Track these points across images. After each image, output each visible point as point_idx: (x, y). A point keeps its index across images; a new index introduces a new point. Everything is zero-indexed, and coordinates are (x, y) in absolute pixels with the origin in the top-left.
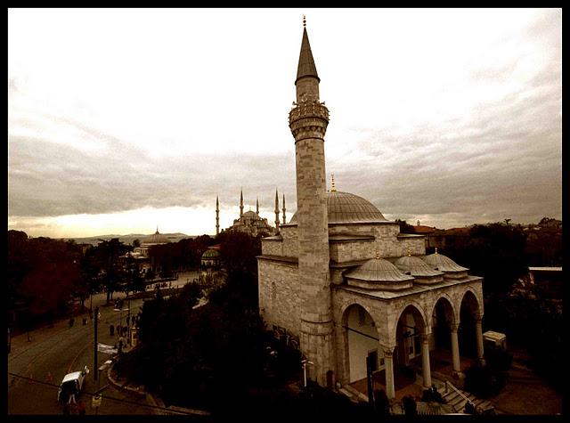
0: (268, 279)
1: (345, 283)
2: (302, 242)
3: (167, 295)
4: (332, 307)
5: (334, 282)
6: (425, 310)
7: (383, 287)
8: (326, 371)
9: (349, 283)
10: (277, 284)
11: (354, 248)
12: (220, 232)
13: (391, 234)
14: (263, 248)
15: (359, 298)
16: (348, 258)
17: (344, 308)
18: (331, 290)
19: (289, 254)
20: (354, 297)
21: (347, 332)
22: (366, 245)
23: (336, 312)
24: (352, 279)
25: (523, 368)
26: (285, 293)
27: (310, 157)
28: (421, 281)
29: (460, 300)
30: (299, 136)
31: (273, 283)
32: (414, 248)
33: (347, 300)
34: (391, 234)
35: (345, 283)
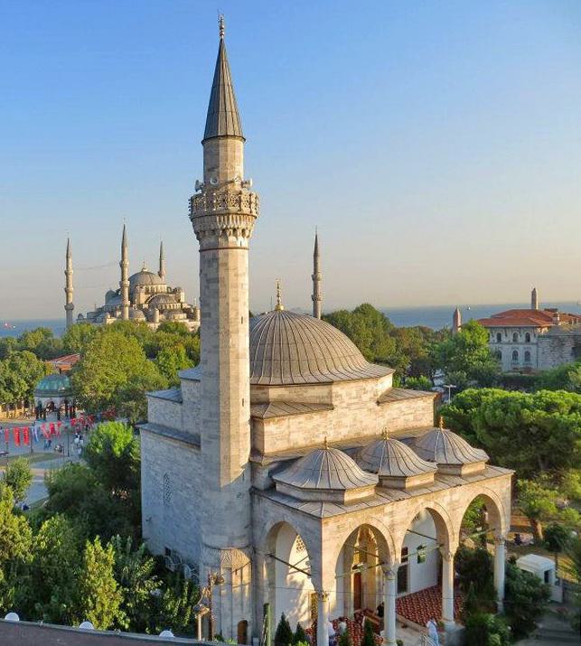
1: (272, 488)
2: (205, 421)
4: (252, 523)
5: (255, 485)
6: (392, 528)
7: (324, 497)
8: (236, 622)
10: (172, 478)
13: (366, 398)
16: (282, 446)
17: (268, 527)
18: (252, 498)
20: (283, 511)
22: (317, 418)
23: (258, 532)
24: (281, 483)
25: (331, 600)
26: (184, 494)
27: (243, 231)
28: (449, 470)
29: (462, 511)
30: (206, 241)
31: (166, 476)
32: (411, 417)
33: (272, 514)
34: (366, 398)
35: (272, 488)
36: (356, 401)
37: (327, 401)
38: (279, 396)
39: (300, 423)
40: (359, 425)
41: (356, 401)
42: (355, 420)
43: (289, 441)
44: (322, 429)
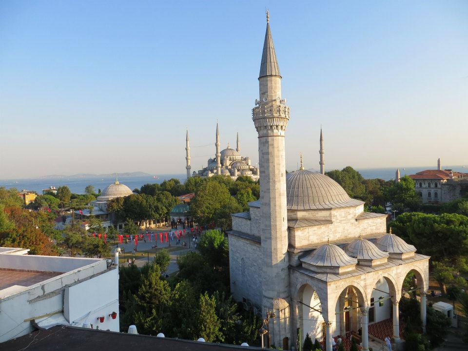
0: (238, 255)
3: (201, 343)
5: (291, 264)
6: (365, 287)
8: (282, 338)
9: (303, 265)
10: (246, 260)
11: (311, 233)
12: (191, 173)
13: (349, 217)
14: (233, 223)
15: (309, 279)
17: (299, 286)
18: (289, 271)
19: (255, 233)
21: (302, 306)
23: (293, 290)
24: (305, 263)
32: (374, 228)
33: (300, 280)
34: (349, 217)
36: (344, 219)
37: (329, 219)
38: (303, 216)
39: (314, 231)
40: (346, 232)
41: (344, 219)
42: (344, 229)
43: (309, 240)
44: (326, 234)
